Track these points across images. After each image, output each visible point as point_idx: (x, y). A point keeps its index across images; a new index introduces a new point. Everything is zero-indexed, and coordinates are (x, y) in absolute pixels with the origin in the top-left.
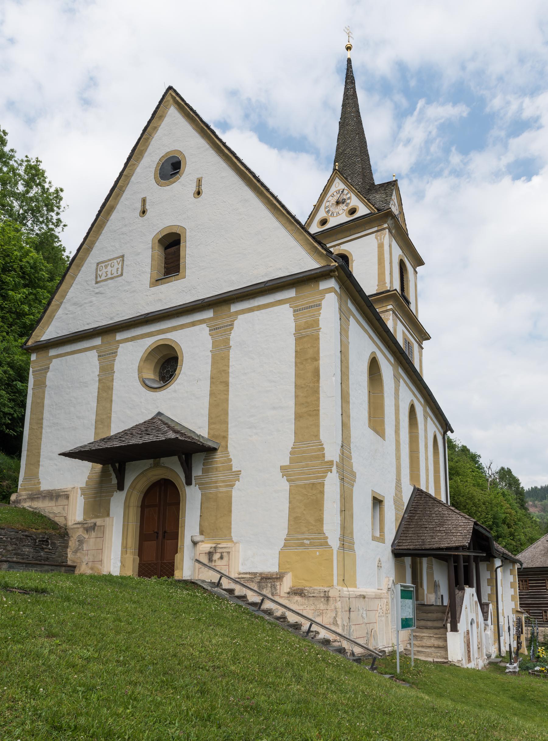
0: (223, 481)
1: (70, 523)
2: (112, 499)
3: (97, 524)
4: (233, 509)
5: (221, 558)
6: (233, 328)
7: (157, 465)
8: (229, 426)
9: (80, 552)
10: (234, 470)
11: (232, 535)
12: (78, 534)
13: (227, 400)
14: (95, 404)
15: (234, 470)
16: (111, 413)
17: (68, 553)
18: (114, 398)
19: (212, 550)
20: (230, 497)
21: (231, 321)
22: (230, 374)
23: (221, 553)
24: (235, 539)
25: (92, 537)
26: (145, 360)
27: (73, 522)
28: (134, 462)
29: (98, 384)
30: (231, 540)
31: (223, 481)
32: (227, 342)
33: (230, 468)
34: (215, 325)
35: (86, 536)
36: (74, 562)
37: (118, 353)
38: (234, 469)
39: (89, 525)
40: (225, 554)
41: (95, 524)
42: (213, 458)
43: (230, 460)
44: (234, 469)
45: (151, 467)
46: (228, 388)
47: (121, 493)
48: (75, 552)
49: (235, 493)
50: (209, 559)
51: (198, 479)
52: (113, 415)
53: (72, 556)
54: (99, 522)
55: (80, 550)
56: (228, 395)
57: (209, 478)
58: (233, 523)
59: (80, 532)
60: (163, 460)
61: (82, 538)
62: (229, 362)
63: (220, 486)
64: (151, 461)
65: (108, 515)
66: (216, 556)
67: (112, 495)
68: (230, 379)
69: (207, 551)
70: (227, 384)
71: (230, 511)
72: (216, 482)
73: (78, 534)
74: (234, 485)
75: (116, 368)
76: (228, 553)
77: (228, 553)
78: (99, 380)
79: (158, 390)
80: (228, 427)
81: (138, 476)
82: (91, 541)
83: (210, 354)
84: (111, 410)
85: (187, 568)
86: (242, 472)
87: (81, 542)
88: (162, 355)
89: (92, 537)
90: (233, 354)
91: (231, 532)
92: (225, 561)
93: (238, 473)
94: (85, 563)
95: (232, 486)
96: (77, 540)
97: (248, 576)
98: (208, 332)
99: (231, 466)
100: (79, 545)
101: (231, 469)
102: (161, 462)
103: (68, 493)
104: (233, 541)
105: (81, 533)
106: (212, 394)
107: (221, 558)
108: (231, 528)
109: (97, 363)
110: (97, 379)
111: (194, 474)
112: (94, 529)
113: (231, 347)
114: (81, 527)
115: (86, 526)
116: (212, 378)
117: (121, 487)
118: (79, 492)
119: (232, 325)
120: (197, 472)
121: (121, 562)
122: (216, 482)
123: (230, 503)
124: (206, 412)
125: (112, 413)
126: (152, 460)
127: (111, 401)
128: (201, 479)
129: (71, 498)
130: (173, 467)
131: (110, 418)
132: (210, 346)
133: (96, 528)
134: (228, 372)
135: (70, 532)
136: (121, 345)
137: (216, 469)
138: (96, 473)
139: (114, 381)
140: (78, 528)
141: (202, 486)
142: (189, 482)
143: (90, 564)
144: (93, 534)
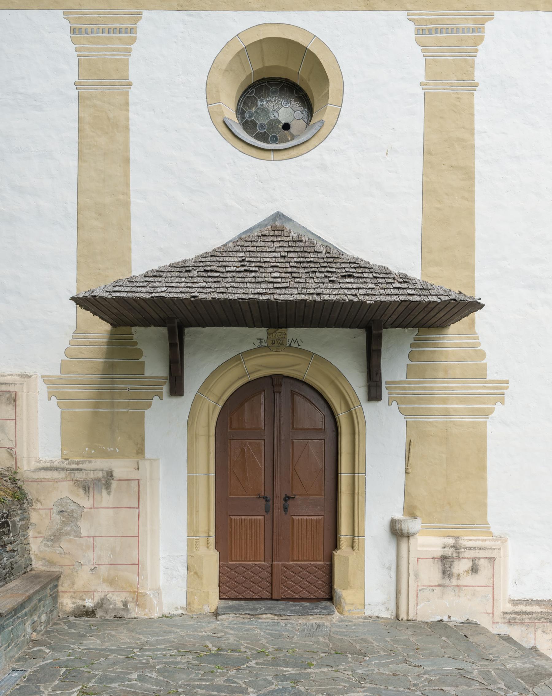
0: (463, 401)
1: (26, 468)
2: (148, 413)
3: (117, 474)
4: (489, 463)
5: (474, 569)
6: (482, 39)
7: (277, 345)
8: (477, 274)
9: (70, 541)
10: (490, 377)
11: (490, 519)
12: (55, 496)
13: (471, 213)
14: (72, 163)
15: (490, 377)
16: (127, 194)
17: (31, 540)
18: (134, 153)
19: (449, 552)
20: (483, 437)
21: (476, 21)
22: (477, 152)
23: (474, 559)
24: (495, 529)
25: (104, 504)
26: (226, 70)
27: (34, 465)
28: (208, 329)
29: (75, 107)
30: (486, 529)
31: (463, 401)
32: (466, 70)
33: (482, 372)
34: (432, 22)
35: (86, 503)
36: (51, 563)
37: (139, 35)
38: (491, 376)
39: (92, 475)
40: (482, 563)
41: (110, 475)
42: (436, 346)
43: (483, 355)
44: (491, 376)
45: (261, 347)
46: (473, 185)
47: (175, 400)
48: (55, 538)
49: (493, 428)
50: (444, 572)
51: (396, 388)
52: (135, 201)
53: (43, 548)
54: (121, 468)
55: (67, 534)
56: (472, 200)
57: (424, 389)
58: (490, 494)
59: (65, 491)
60: (293, 333)
61: (72, 507)
62: (472, 122)
63: (455, 410)
64: (262, 332)
65: (140, 451)
66: (461, 566)
67: (149, 406)
68: (477, 162)
69: (438, 554)
70: (468, 174)
71: (482, 467)
72: (444, 401)
73: (55, 496)
74: (492, 411)
75: (133, 74)
76: (492, 560)
77: (492, 560)
78: (81, 99)
79: (271, 155)
80: (473, 278)
81: (216, 364)
82: (101, 515)
83: (420, 92)
84: (128, 185)
85: (371, 581)
86: (511, 384)
87: (69, 515)
88: (282, 64)
89: (104, 504)
90: (481, 102)
91: (485, 514)
92: (482, 578)
93: (500, 388)
94: (87, 568)
95: (487, 413)
96: (56, 509)
97: (536, 609)
98: (413, 36)
99: (484, 368)
100: (64, 523)
101: (484, 376)
102: (290, 338)
103: (12, 389)
104: (491, 533)
105: (66, 494)
106: (427, 192)
107: (474, 569)
108: (485, 505)
109: (71, 48)
110: (75, 93)
111: (386, 376)
112: (108, 485)
113: (477, 85)
114: (64, 480)
115: (79, 476)
116: (427, 152)
117: (176, 388)
118: (42, 388)
119: (480, 30)
120: (393, 369)
121: (188, 567)
122: (444, 401)
123: (482, 451)
124: (415, 232)
125: (132, 194)
126: (265, 329)
127: (127, 161)
128: (404, 389)
129: (22, 402)
130: (337, 356)
131: (126, 205)
132: (420, 73)
133: (114, 484)
134: (473, 147)
135: (30, 490)
136: (145, 13)
137: (446, 371)
138: (91, 344)
139: (131, 108)
140: (57, 481)
141: (410, 408)
142: (374, 393)
143: (103, 570)
144: (106, 499)
